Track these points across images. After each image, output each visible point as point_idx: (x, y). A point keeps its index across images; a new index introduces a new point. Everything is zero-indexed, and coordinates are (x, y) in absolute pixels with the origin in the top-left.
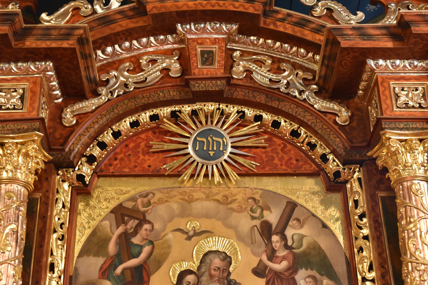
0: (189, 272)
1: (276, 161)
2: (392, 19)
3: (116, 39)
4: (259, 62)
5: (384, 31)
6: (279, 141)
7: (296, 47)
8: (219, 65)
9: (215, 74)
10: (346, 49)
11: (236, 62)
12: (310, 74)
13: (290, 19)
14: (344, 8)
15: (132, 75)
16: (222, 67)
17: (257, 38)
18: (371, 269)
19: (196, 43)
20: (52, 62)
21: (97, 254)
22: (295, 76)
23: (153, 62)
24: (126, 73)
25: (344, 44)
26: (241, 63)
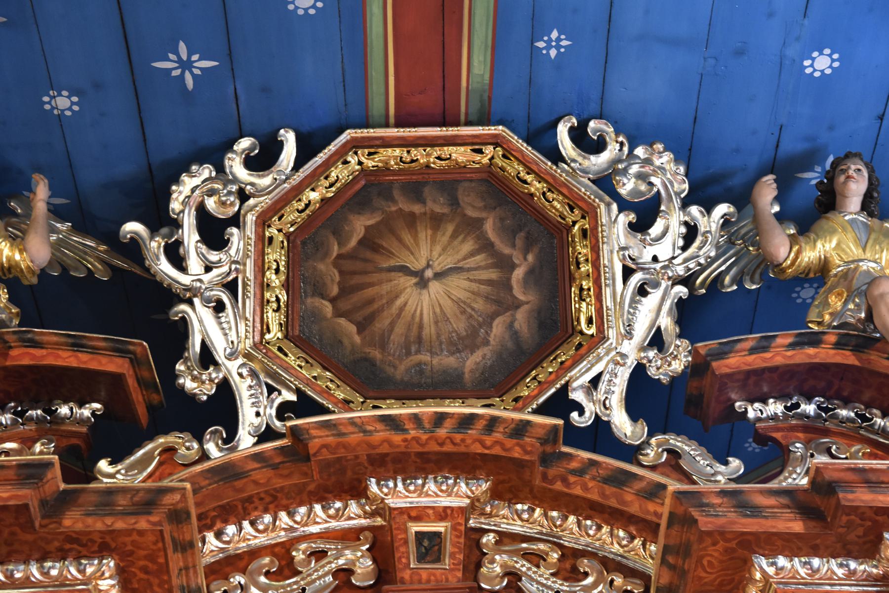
2: (799, 474)
3: (245, 509)
4: (533, 557)
5: (784, 500)
7: (609, 527)
8: (452, 561)
9: (444, 580)
10: (709, 533)
11: (487, 556)
12: (638, 582)
13: (595, 470)
14: (701, 450)
15: (274, 583)
16: (458, 567)
17: (529, 507)
19: (406, 517)
20: (113, 558)
22: (608, 586)
23: (318, 554)
24: (263, 579)
25: (705, 523)
26: (497, 557)
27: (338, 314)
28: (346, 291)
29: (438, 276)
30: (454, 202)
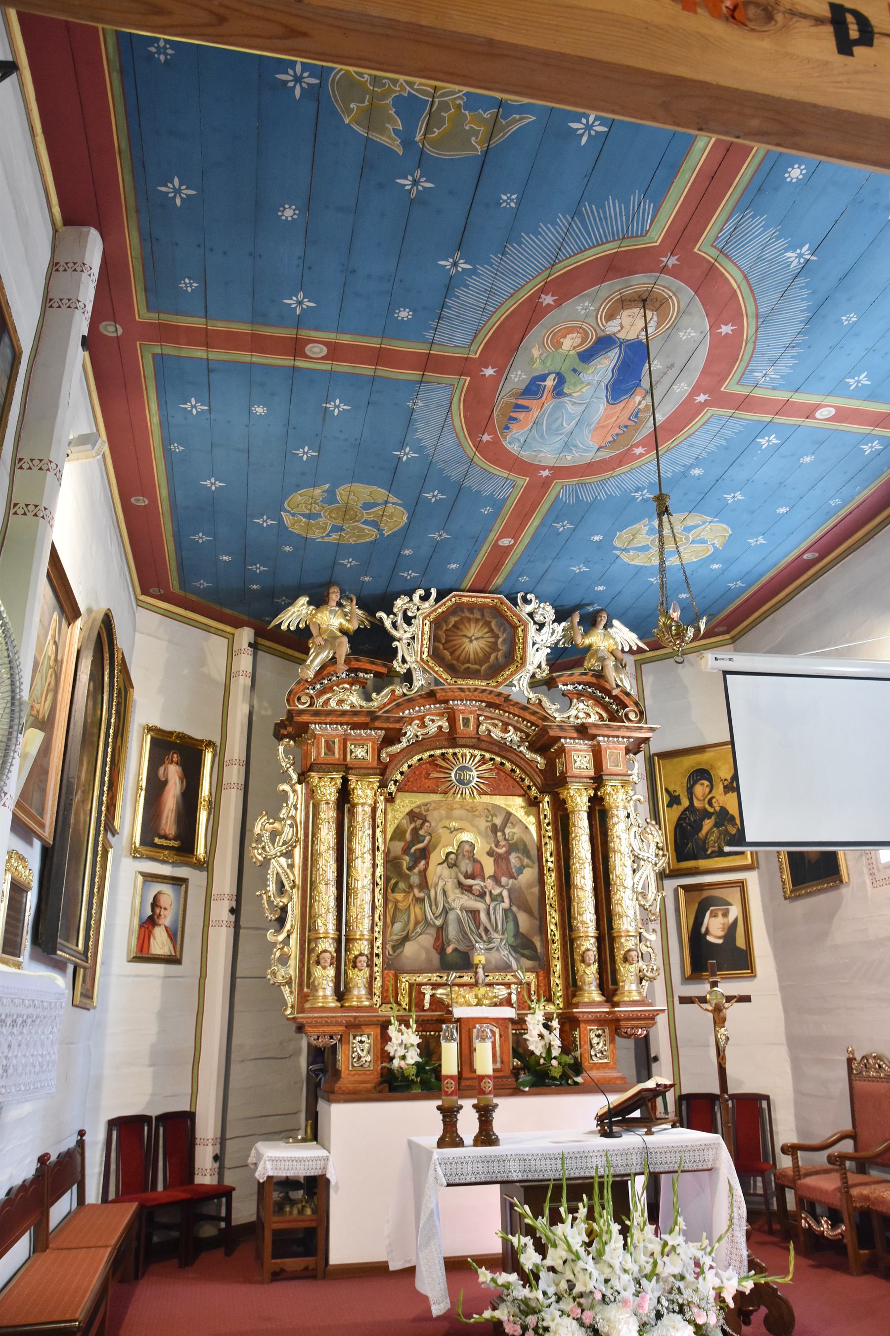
0: (451, 853)
1: (501, 787)
6: (502, 774)
18: (551, 855)
21: (400, 840)
27: (445, 649)
28: (447, 641)
29: (476, 639)
30: (483, 615)
